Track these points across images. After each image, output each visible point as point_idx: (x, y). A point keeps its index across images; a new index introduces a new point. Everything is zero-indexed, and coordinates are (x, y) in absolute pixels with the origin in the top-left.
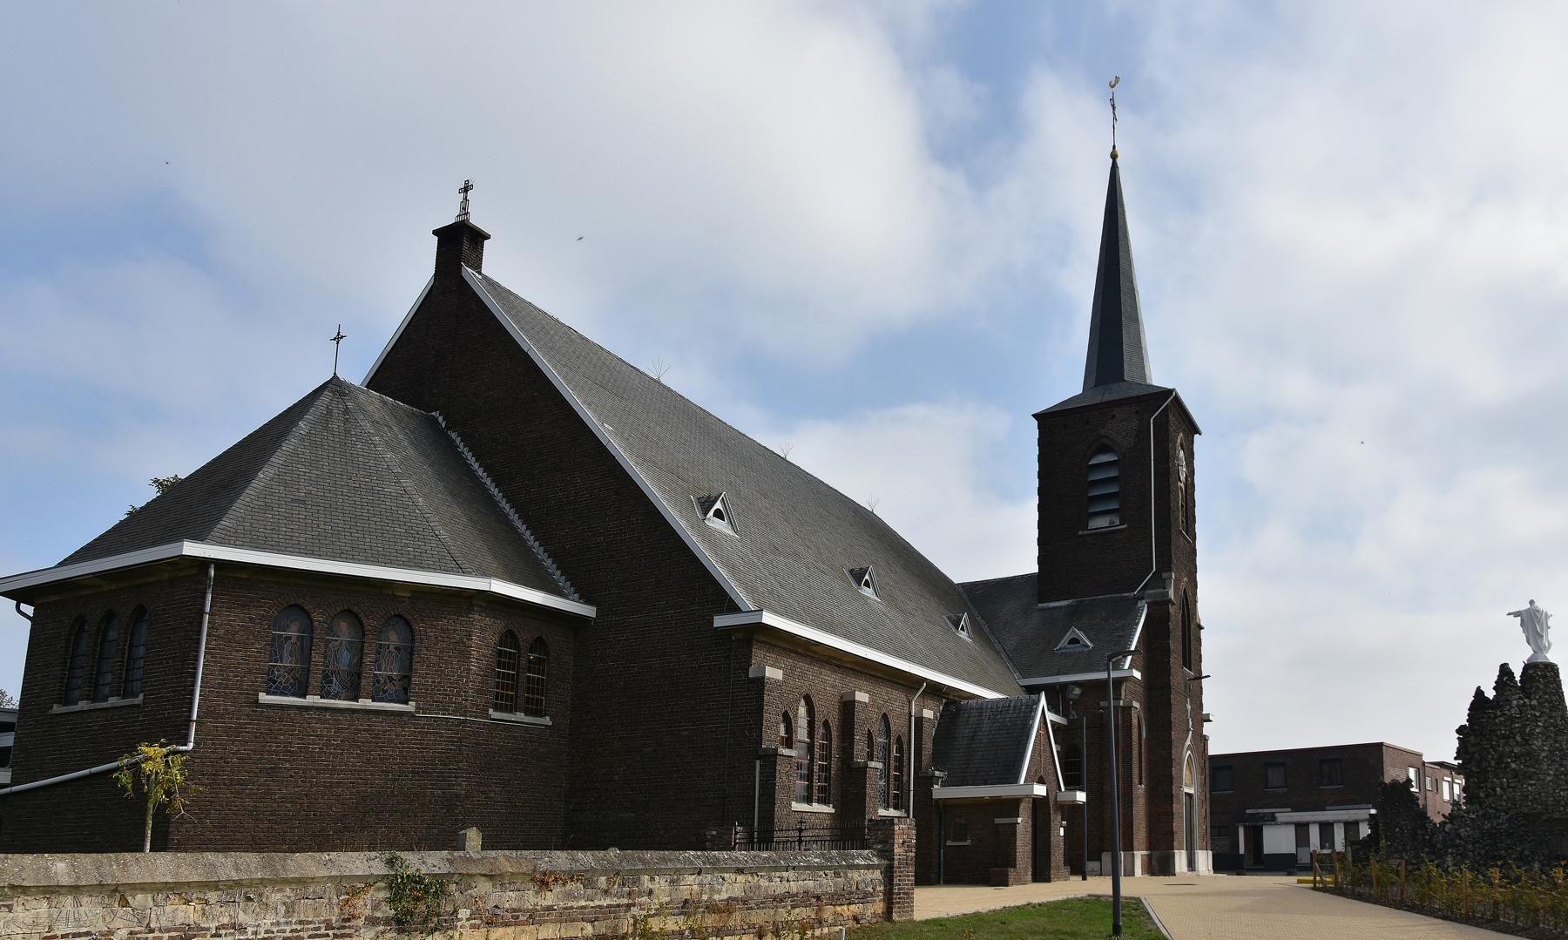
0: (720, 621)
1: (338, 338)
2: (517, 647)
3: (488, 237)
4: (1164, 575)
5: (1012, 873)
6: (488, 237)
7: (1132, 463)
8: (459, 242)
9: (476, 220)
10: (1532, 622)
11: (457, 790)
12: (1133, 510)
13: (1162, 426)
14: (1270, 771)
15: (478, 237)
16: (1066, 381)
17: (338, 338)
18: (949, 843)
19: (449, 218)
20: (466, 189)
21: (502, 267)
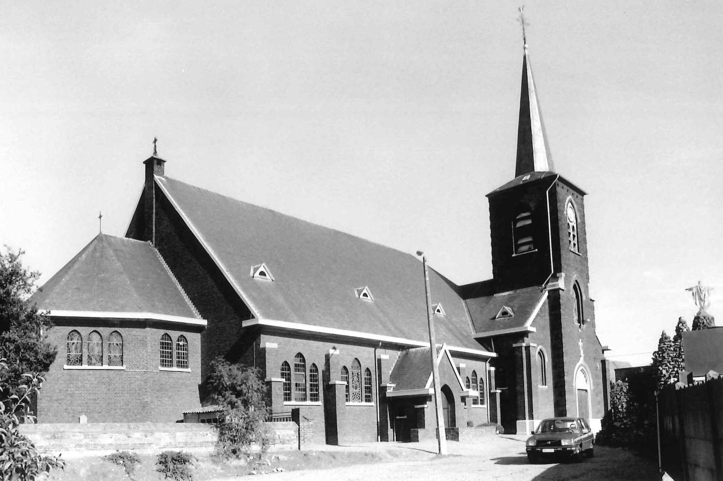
0: (246, 324)
1: (100, 217)
2: (171, 340)
3: (165, 162)
4: (558, 275)
5: (421, 432)
6: (165, 162)
7: (539, 216)
8: (153, 165)
9: (160, 156)
10: (698, 293)
11: (146, 400)
12: (540, 241)
13: (553, 194)
14: (704, 377)
15: (160, 162)
16: (503, 173)
17: (100, 217)
18: (398, 417)
19: (149, 155)
20: (155, 141)
21: (174, 171)
